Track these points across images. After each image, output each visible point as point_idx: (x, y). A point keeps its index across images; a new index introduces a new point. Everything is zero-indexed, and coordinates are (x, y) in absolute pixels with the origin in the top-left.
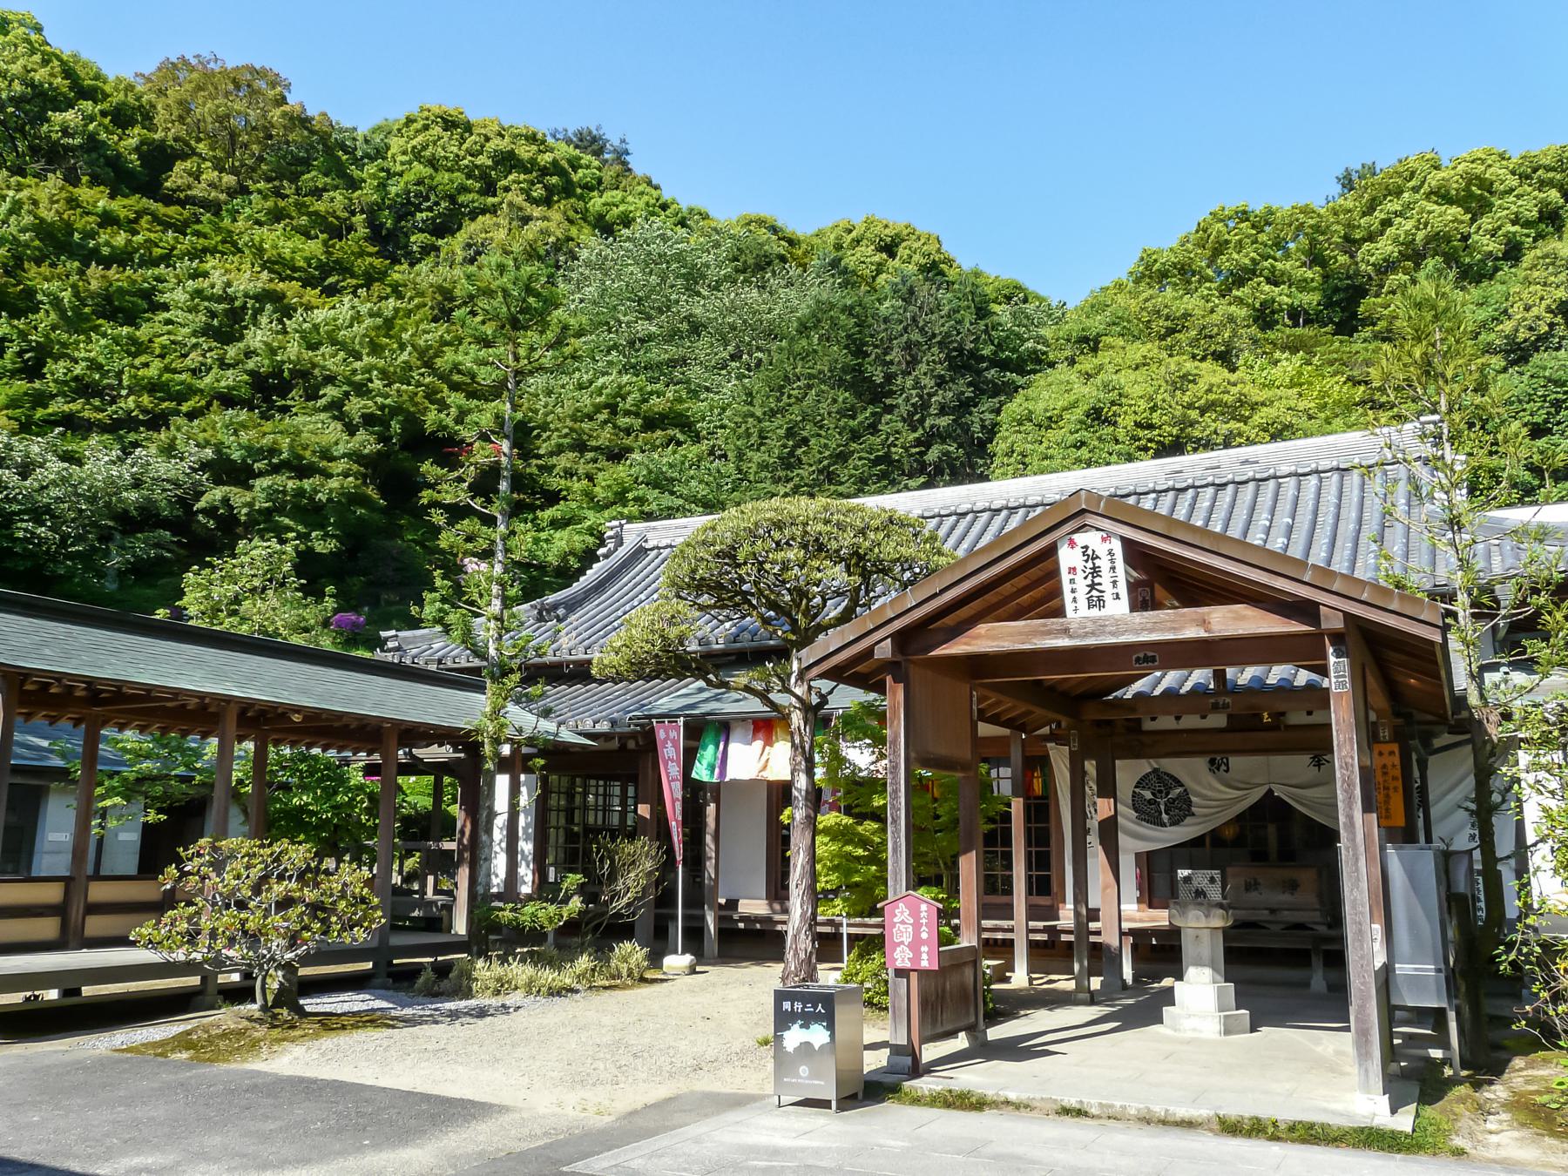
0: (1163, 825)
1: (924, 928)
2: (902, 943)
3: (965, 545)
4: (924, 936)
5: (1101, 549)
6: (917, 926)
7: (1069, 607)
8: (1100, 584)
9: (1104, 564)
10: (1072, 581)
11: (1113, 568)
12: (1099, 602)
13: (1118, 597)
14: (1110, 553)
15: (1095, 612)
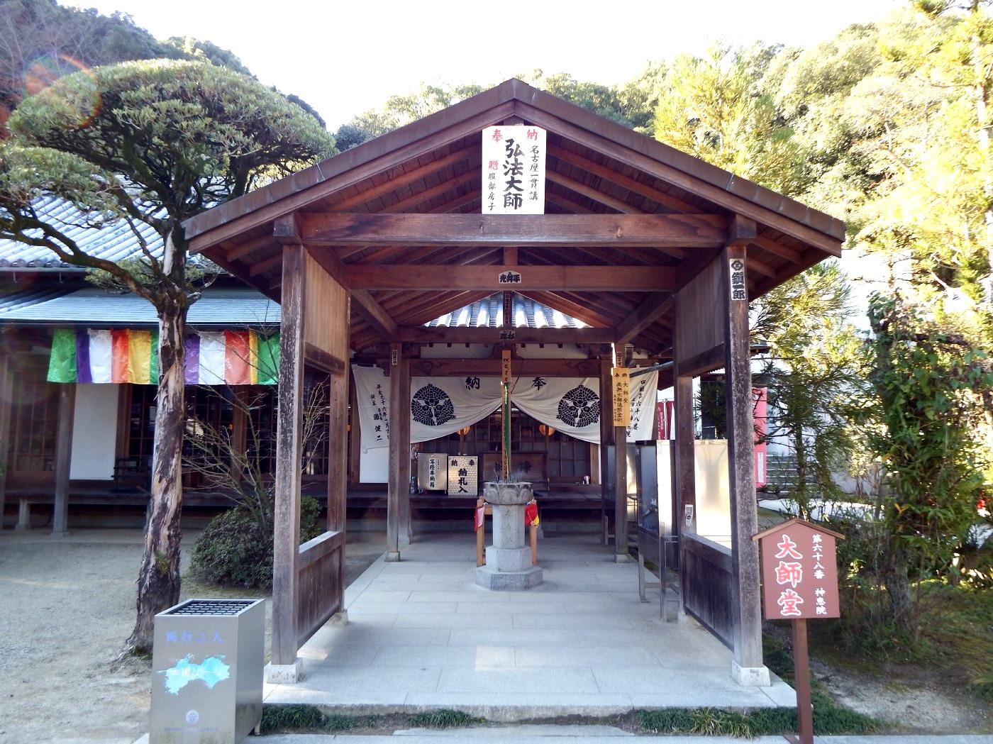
0: (432, 424)
1: (818, 565)
2: (789, 585)
4: (819, 575)
6: (808, 565)
8: (519, 182)
9: (526, 161)
11: (535, 167)
12: (517, 201)
13: (535, 197)
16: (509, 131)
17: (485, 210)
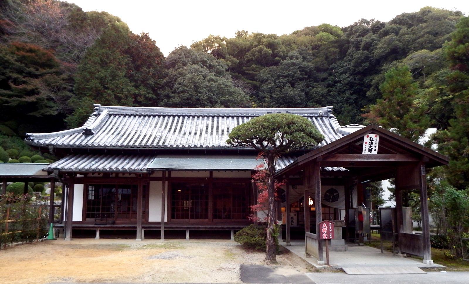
3: (225, 133)
5: (374, 139)
6: (328, 229)
7: (363, 151)
9: (374, 142)
10: (366, 145)
11: (376, 143)
12: (371, 151)
14: (376, 140)
15: (369, 153)
16: (370, 136)
17: (363, 153)
